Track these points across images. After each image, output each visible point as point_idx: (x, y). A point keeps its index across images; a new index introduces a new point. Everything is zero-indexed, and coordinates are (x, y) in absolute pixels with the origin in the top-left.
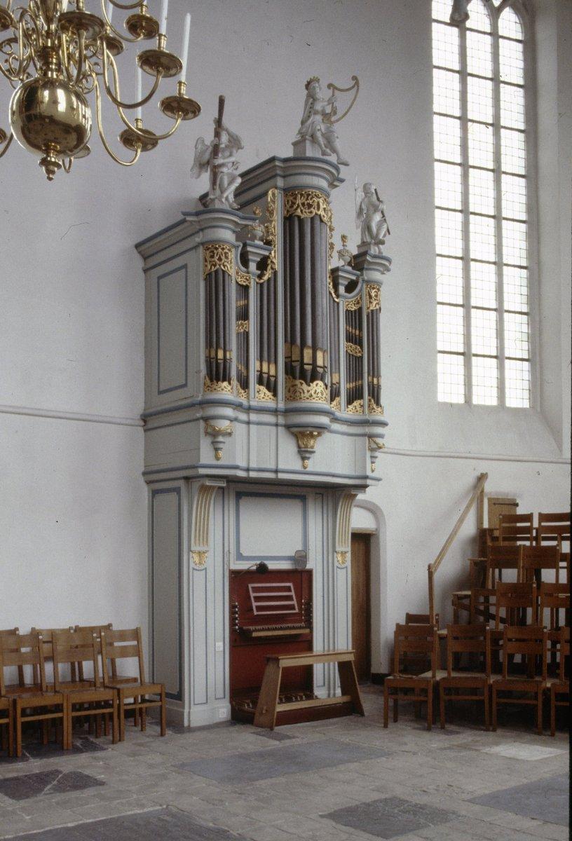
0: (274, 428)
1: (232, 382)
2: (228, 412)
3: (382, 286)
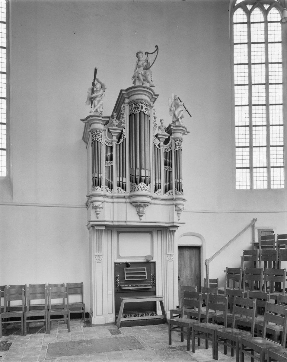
1: (102, 186)
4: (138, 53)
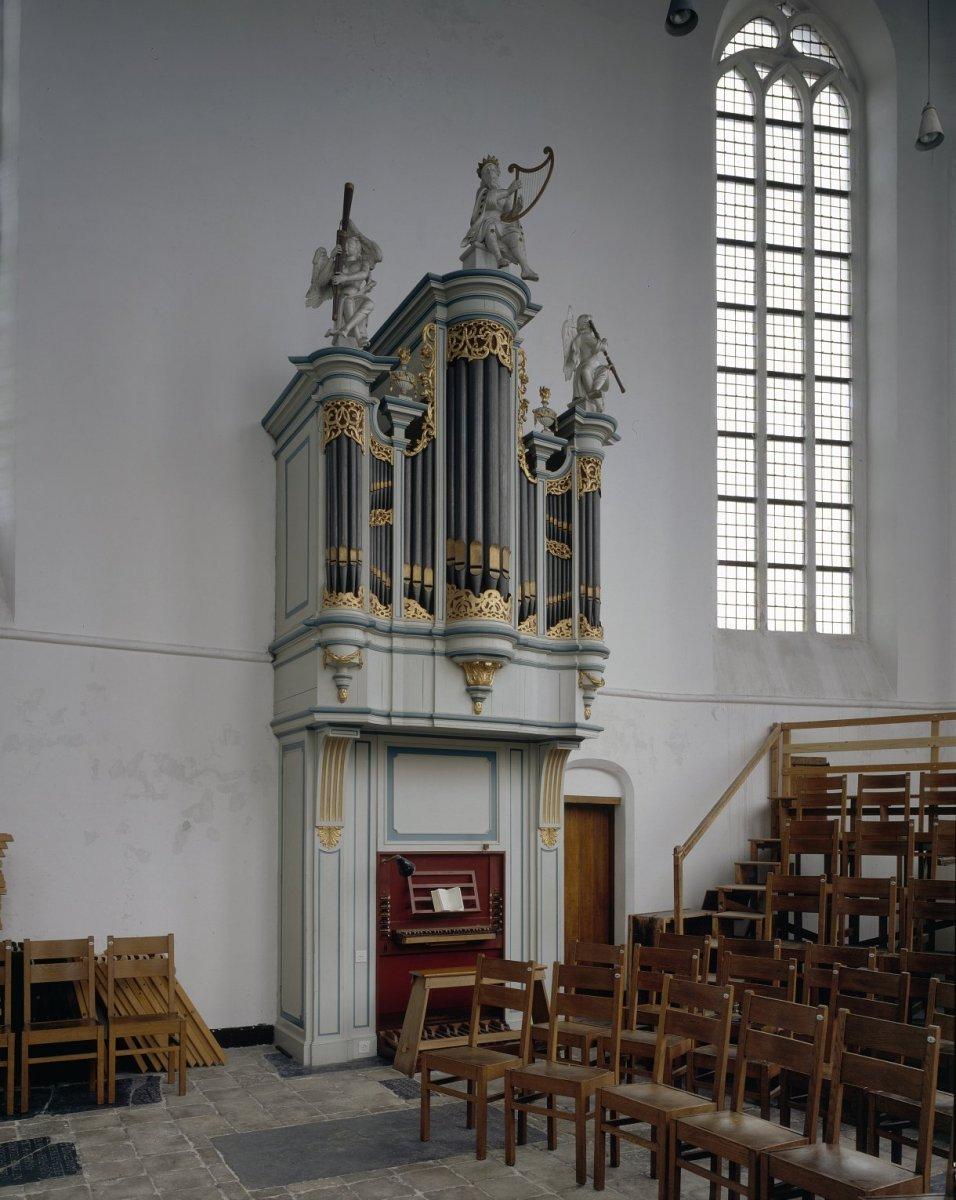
0: (430, 658)
1: (360, 593)
2: (356, 634)
3: (604, 465)
4: (485, 162)
